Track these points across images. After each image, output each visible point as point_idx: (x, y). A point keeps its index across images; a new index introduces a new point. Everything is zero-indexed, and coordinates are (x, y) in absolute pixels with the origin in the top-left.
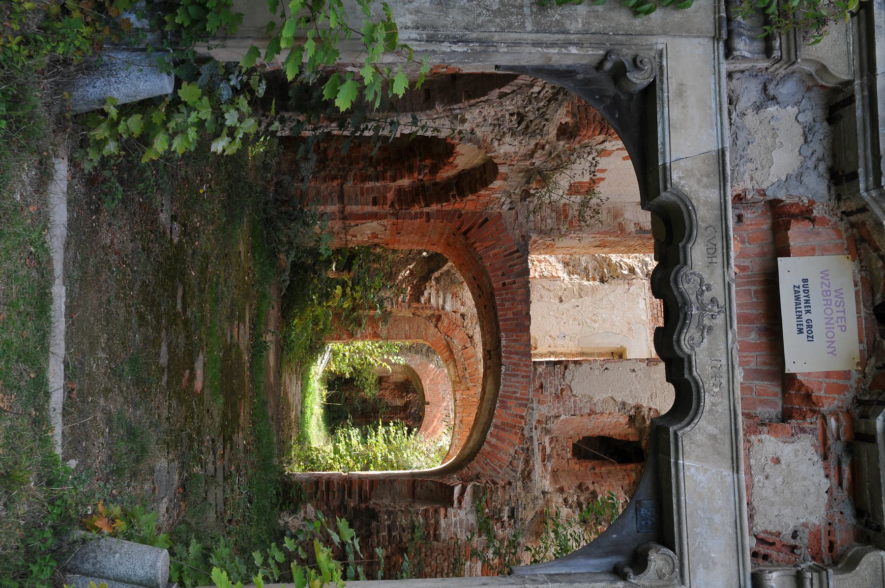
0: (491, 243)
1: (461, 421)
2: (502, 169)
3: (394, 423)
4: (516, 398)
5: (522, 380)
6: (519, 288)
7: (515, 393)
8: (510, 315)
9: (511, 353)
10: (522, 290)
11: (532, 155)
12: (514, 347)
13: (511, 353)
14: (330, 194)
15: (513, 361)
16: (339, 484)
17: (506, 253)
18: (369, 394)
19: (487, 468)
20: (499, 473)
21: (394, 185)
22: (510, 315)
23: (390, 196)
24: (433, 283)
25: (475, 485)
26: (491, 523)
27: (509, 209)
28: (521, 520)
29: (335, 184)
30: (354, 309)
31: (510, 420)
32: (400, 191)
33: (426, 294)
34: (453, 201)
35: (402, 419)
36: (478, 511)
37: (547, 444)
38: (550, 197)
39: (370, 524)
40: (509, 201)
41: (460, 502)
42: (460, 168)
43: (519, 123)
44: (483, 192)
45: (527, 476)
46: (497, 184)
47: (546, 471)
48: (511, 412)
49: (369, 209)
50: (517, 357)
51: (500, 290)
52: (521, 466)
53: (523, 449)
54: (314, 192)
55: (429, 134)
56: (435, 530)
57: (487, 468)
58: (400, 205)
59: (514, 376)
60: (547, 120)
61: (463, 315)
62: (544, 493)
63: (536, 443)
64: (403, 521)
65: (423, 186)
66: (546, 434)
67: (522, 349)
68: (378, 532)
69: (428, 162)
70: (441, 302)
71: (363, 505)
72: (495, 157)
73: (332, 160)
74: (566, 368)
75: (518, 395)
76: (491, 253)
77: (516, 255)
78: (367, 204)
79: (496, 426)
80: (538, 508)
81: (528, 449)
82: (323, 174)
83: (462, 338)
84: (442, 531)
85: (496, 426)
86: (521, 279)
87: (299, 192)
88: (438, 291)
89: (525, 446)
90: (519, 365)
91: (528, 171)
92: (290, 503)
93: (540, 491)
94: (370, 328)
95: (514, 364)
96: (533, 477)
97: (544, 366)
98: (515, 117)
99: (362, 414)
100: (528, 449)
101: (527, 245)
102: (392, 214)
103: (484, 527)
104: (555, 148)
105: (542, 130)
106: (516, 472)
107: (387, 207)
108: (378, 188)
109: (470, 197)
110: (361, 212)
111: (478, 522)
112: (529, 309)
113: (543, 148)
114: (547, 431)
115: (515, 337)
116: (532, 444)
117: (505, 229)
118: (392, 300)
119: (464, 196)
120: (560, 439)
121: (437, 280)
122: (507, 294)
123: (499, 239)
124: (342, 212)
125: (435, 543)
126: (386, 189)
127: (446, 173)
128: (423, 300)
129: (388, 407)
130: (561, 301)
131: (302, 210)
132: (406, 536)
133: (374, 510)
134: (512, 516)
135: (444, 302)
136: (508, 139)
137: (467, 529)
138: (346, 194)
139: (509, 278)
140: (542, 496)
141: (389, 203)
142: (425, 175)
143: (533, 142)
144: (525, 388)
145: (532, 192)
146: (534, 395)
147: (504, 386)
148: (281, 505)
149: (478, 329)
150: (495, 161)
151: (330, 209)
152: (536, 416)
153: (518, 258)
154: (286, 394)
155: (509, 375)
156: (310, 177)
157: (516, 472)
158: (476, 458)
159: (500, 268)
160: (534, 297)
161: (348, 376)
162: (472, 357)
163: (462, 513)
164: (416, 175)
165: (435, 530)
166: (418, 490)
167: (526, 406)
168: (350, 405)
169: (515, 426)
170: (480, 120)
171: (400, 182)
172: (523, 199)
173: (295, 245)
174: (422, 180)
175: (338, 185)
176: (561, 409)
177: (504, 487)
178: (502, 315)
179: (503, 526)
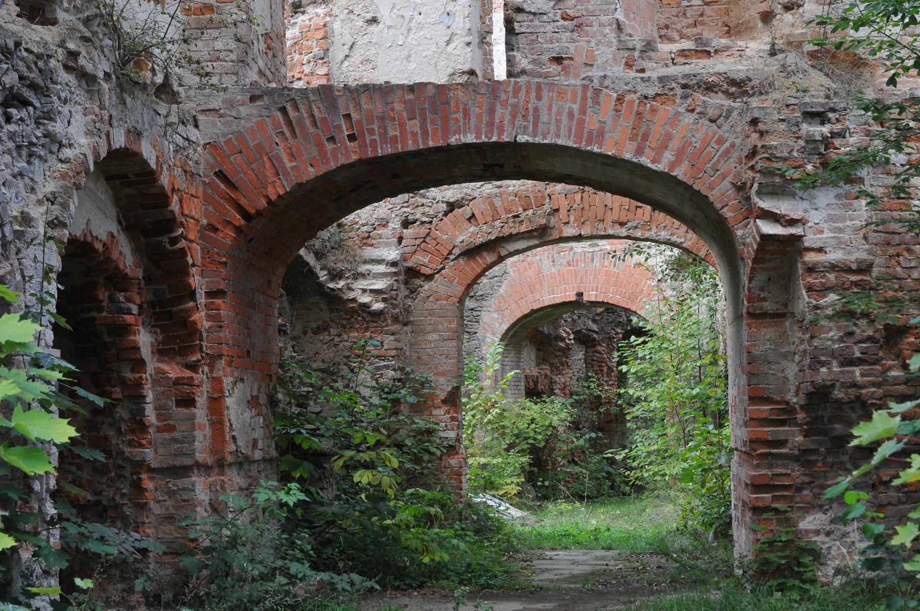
0: (268, 165)
1: (622, 224)
2: (120, 140)
3: (620, 363)
4: (583, 111)
5: (545, 100)
6: (358, 106)
7: (571, 114)
8: (414, 126)
9: (491, 124)
10: (363, 100)
11: (87, 78)
12: (479, 117)
13: (491, 124)
14: (171, 494)
15: (508, 117)
16: (758, 466)
17: (288, 134)
18: (563, 415)
19: (723, 168)
20: (733, 145)
21: (152, 365)
22: (414, 126)
23: (174, 371)
24: (341, 284)
25: (759, 193)
26: (835, 157)
27: (196, 126)
28: (828, 97)
29: (149, 485)
30: (399, 446)
31: (626, 123)
32: (163, 352)
33: (365, 299)
34: (183, 244)
35: (611, 351)
36: (811, 184)
37: (675, 47)
38: (172, 42)
39: (838, 402)
40: (181, 129)
41: (792, 222)
42: (114, 228)
43: (25, 103)
44: (165, 180)
45: (738, 87)
46: (148, 152)
47: (727, 48)
48: (610, 123)
49: (201, 413)
50: (499, 110)
51: (363, 146)
52: (717, 101)
53: (684, 97)
54: (168, 528)
55: (53, 287)
56: (849, 271)
57: (723, 168)
58: (191, 350)
59: (537, 117)
60: (18, 44)
61: (406, 224)
62: (773, 53)
63: (672, 70)
64: (831, 335)
65: (152, 305)
66: (654, 50)
67: (485, 101)
68: (854, 385)
69: (103, 295)
70: (381, 268)
71: (801, 416)
72: (96, 154)
73: (98, 493)
74: (519, 10)
75: (576, 107)
76: (289, 165)
77: (292, 114)
78: (193, 417)
79: (639, 151)
80: (805, 64)
81: (685, 86)
82: (128, 511)
83: (455, 224)
84: (852, 258)
85: (639, 151)
86: (341, 103)
87: (167, 559)
88: (357, 276)
89: (679, 91)
90: (515, 106)
91: (120, 86)
92: (799, 564)
93: (771, 60)
94: (435, 412)
95: (514, 116)
96: (742, 76)
97: (518, 55)
98: (14, 111)
99: (601, 429)
100: (685, 86)
101: (271, 92)
102: (212, 367)
103: (841, 173)
104: (72, 29)
105: (39, 56)
106: (730, 111)
107: (199, 377)
108: (156, 398)
109: (175, 206)
110: (208, 431)
111: (835, 184)
112: (401, 87)
113: (73, 55)
114: (649, 47)
115: (460, 115)
116: (674, 79)
117: (240, 136)
118: (378, 368)
119: (174, 219)
120: (663, 21)
121: (336, 275)
122: (372, 132)
123: (260, 147)
124: (206, 469)
125: (875, 271)
126: (160, 379)
127: (126, 257)
128: (378, 306)
129: (587, 378)
130: (374, 20)
131: (207, 551)
132: (863, 329)
133: (809, 395)
134: (820, 117)
135: (379, 262)
136: (57, 127)
137: (847, 207)
138: (171, 462)
139: (338, 127)
140: (780, 56)
141: (187, 373)
142: (129, 300)
143: (64, 77)
144: (561, 94)
145: (159, 79)
146: (576, 76)
147: (558, 136)
148: (804, 582)
149: (434, 192)
150: (103, 154)
151: (202, 494)
152: (618, 70)
153: (297, 108)
154: (573, 578)
155: (535, 125)
156: (138, 536)
157: (730, 111)
158: (704, 192)
159: (320, 146)
160: (378, 78)
161: (525, 459)
162: (492, 204)
163: (815, 217)
164: (129, 318)
165: (849, 271)
166: (768, 306)
167: (597, 92)
168: (585, 457)
169: (638, 113)
170: (21, 185)
171: (146, 352)
172: (174, 98)
173: (279, 563)
174: (140, 307)
175: (152, 479)
176: (604, 19)
177: (762, 134)
178: (415, 141)
179: (841, 135)
